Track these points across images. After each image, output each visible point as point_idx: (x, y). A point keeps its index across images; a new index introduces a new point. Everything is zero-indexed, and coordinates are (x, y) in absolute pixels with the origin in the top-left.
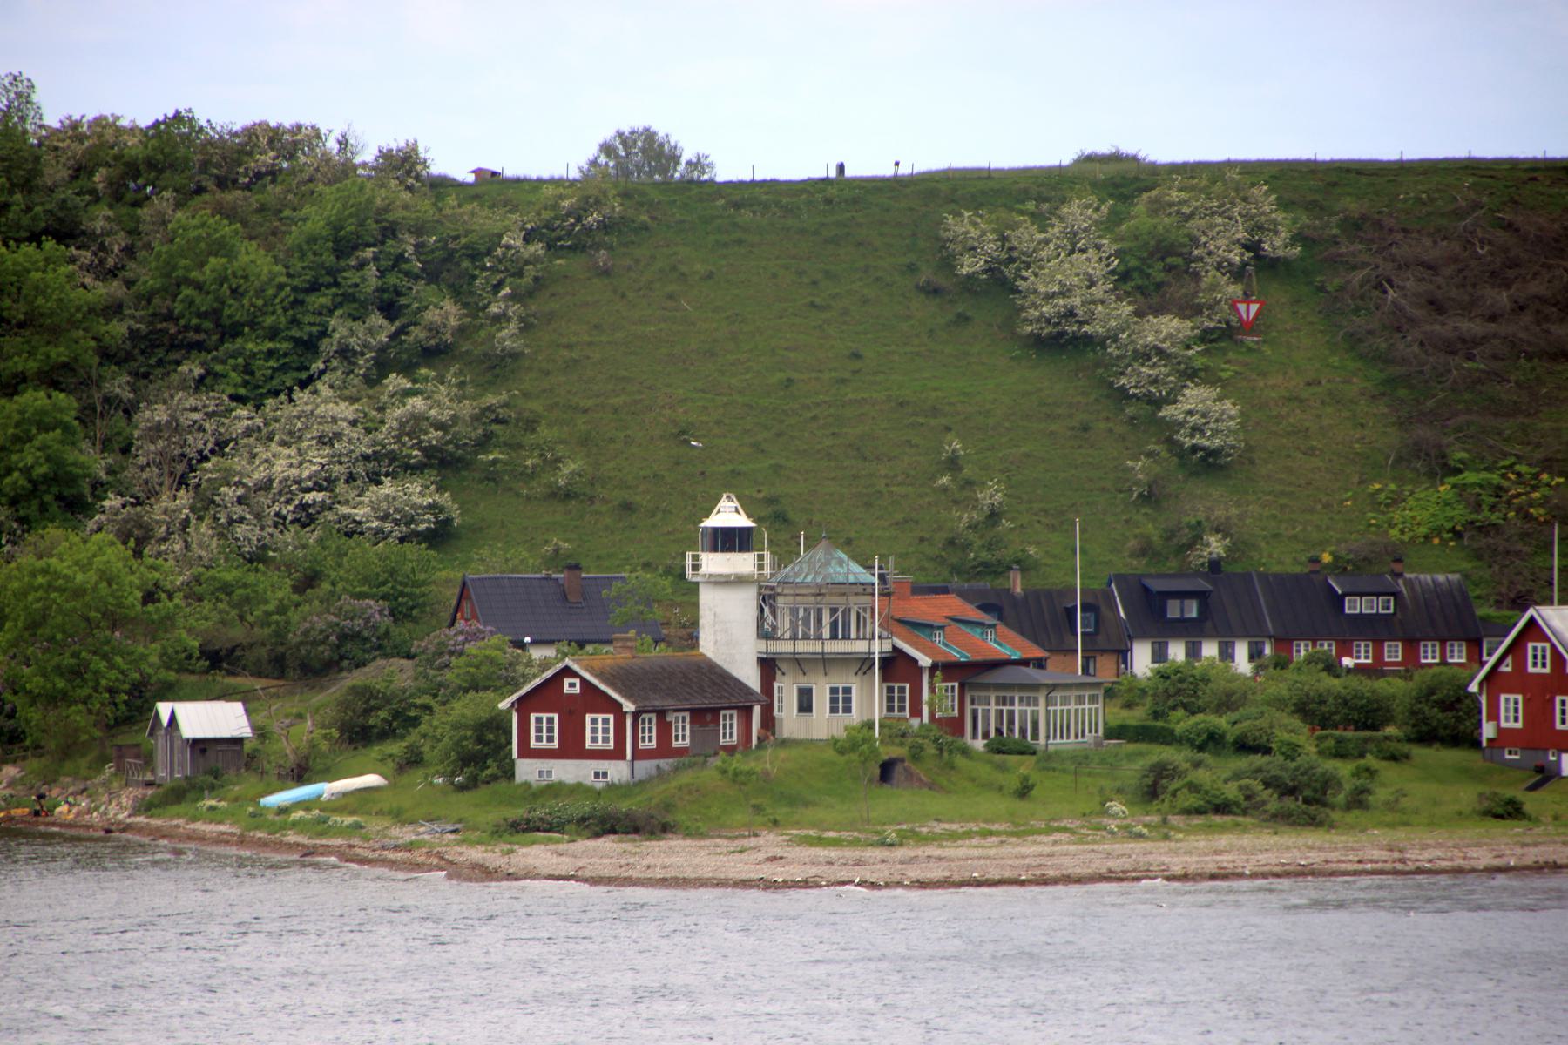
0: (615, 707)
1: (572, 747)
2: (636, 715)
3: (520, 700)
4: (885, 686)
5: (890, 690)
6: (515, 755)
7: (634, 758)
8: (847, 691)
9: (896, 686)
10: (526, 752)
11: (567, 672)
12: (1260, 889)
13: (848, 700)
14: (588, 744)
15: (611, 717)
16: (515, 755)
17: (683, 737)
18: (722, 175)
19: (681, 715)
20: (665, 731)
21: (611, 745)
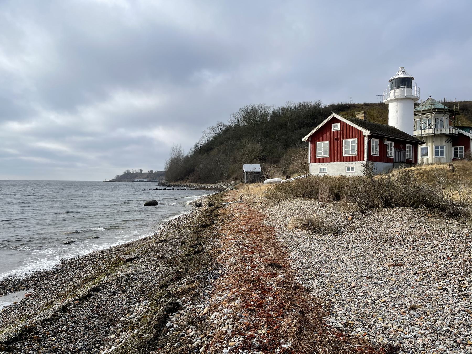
0: (359, 135)
1: (336, 155)
2: (369, 137)
3: (311, 136)
4: (453, 148)
5: (456, 149)
6: (309, 162)
7: (368, 160)
8: (442, 148)
9: (458, 147)
10: (315, 160)
11: (335, 120)
12: (15, 255)
13: (442, 151)
14: (344, 155)
15: (356, 140)
16: (309, 162)
17: (391, 152)
18: (322, 106)
19: (390, 142)
20: (383, 148)
21: (356, 154)
